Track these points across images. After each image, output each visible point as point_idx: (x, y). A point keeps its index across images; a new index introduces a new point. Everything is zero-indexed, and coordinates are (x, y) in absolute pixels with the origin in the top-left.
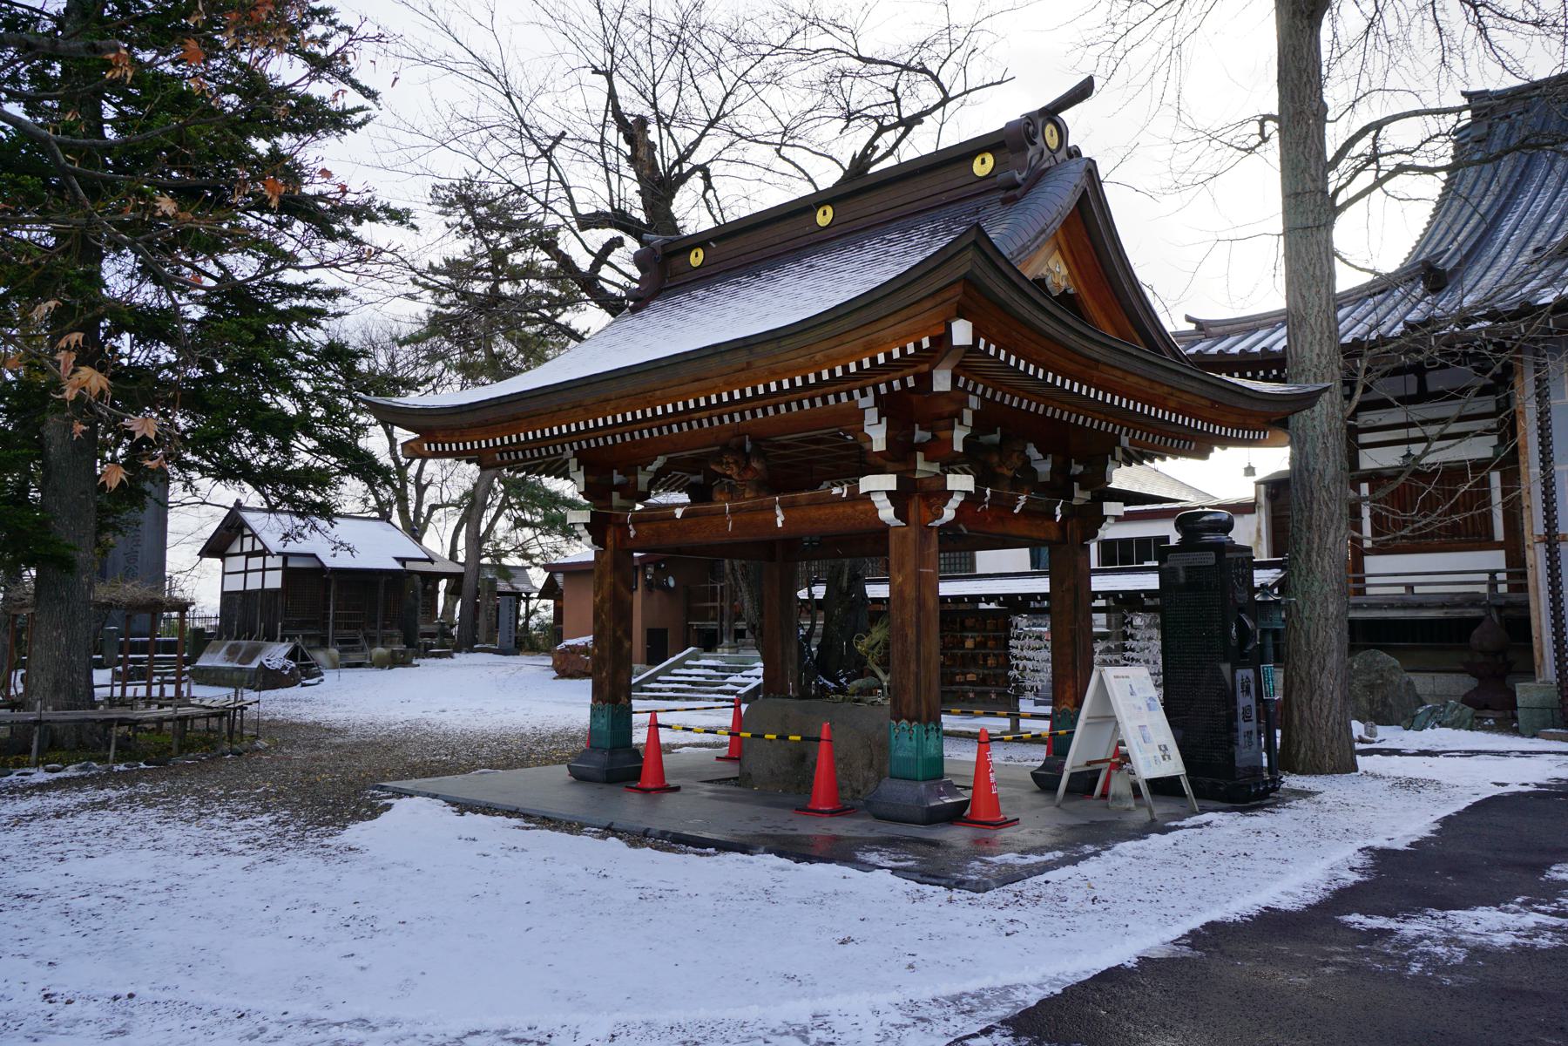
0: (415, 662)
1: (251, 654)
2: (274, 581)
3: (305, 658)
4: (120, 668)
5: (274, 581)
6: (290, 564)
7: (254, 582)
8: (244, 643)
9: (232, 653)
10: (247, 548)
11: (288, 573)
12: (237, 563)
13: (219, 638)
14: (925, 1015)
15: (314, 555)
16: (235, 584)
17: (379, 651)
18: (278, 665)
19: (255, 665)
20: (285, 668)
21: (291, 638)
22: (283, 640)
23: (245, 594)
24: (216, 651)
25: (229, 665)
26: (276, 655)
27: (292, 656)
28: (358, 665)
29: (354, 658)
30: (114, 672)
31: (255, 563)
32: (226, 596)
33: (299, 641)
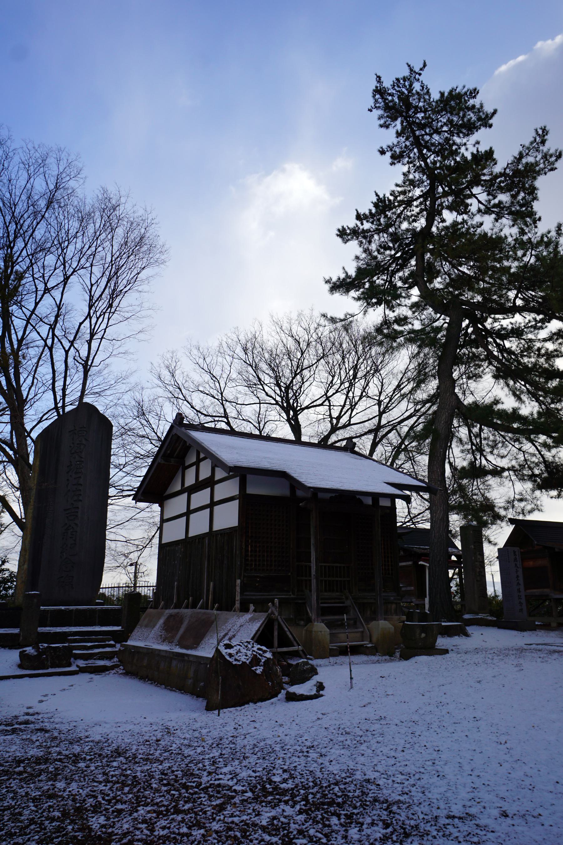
0: (442, 642)
1: (196, 636)
2: (228, 517)
3: (284, 641)
4: (29, 650)
5: (228, 517)
6: (250, 490)
7: (199, 525)
8: (187, 612)
9: (170, 630)
10: (190, 480)
11: (247, 502)
12: (178, 505)
13: (156, 607)
14: (366, 709)
15: (284, 475)
16: (175, 532)
17: (383, 626)
18: (244, 657)
19: (206, 651)
20: (255, 660)
21: (261, 606)
22: (244, 609)
23: (189, 543)
24: (150, 625)
25: (164, 647)
26: (238, 636)
27: (262, 638)
28: (355, 651)
29: (348, 638)
30: (23, 656)
31: (201, 498)
32: (166, 552)
33: (274, 610)
